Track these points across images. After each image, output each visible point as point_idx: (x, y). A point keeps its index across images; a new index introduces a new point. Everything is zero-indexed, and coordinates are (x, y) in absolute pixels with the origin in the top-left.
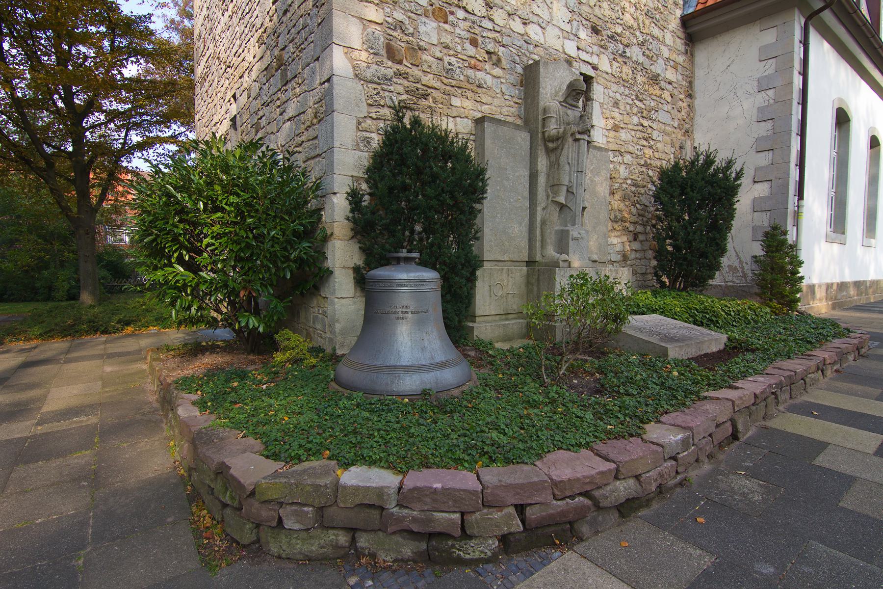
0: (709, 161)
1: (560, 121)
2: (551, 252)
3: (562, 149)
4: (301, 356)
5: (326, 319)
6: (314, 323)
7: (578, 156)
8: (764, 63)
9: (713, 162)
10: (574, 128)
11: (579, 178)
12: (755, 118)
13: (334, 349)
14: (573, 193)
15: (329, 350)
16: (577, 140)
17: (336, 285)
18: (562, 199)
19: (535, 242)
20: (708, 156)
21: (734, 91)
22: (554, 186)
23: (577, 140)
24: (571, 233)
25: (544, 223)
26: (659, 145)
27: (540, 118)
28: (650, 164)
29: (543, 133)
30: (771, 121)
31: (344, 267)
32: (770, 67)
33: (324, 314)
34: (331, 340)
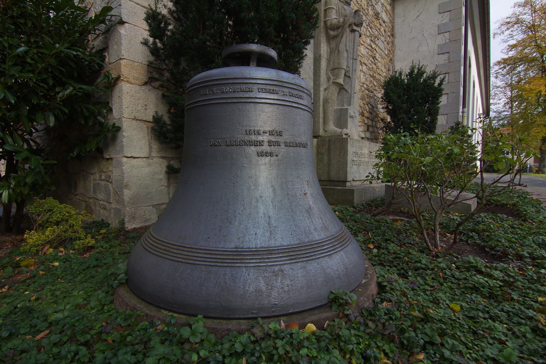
0: (421, 73)
1: (339, 12)
2: (332, 127)
3: (342, 37)
4: (70, 233)
5: (110, 185)
6: (95, 192)
7: (354, 45)
8: (442, 15)
9: (423, 73)
10: (351, 20)
11: (354, 65)
12: (436, 52)
13: (122, 223)
14: (349, 77)
15: (114, 224)
16: (353, 31)
17: (125, 140)
18: (341, 81)
19: (319, 119)
20: (419, 69)
21: (422, 33)
22: (334, 70)
23: (353, 31)
24: (349, 111)
25: (326, 101)
26: (379, 64)
27: (323, 9)
28: (375, 77)
29: (325, 22)
30: (447, 54)
31: (135, 119)
32: (446, 18)
33: (108, 180)
34: (118, 211)
